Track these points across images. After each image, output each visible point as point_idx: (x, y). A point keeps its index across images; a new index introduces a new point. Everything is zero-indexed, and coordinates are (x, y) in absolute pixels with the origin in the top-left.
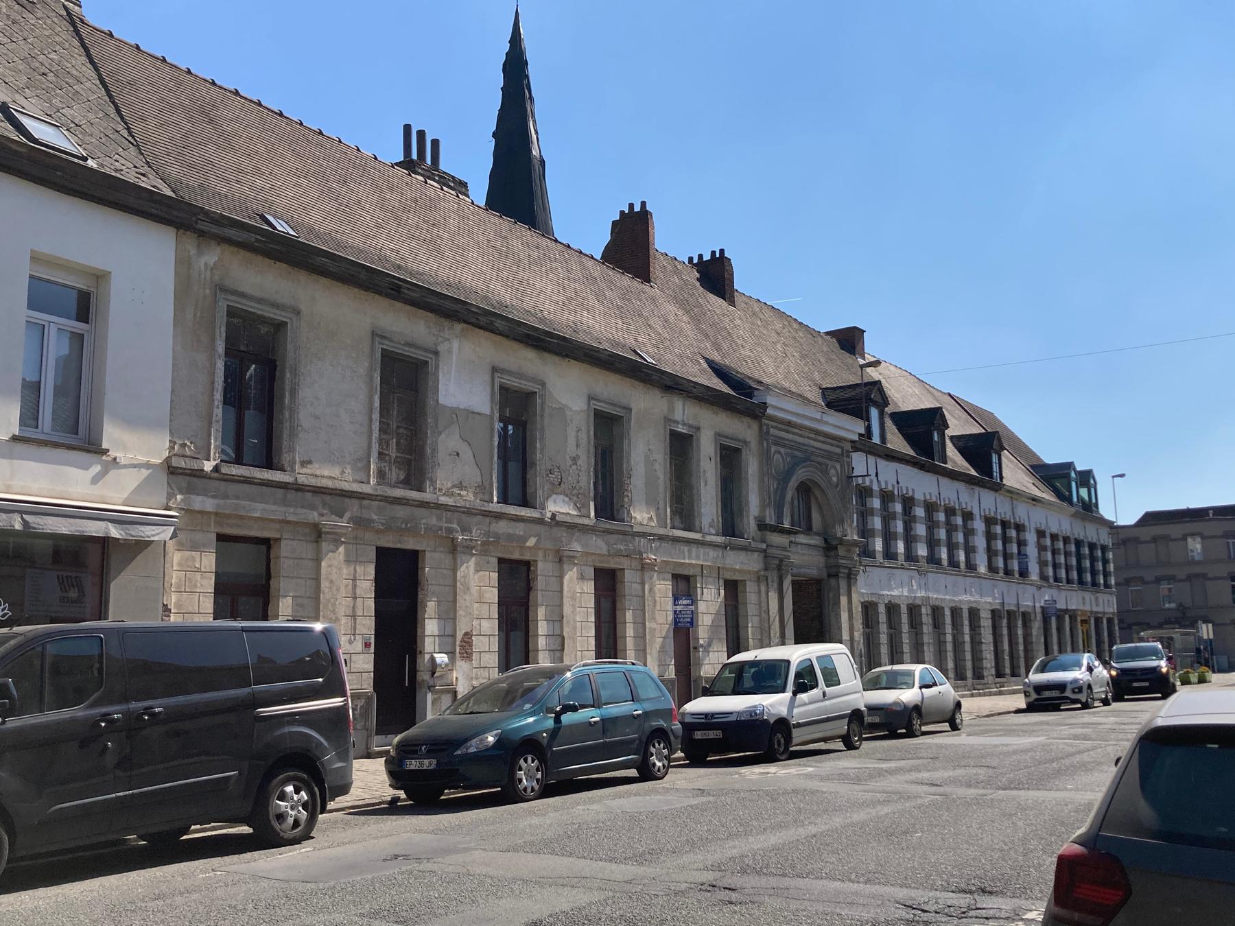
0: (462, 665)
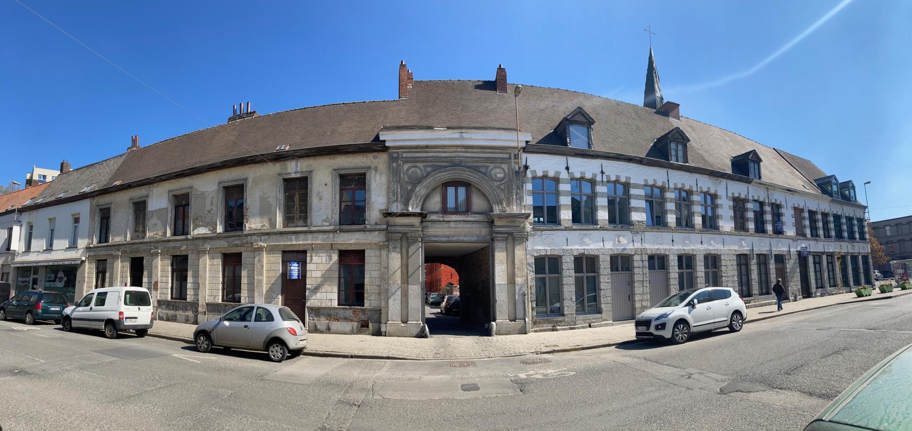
0: (154, 292)
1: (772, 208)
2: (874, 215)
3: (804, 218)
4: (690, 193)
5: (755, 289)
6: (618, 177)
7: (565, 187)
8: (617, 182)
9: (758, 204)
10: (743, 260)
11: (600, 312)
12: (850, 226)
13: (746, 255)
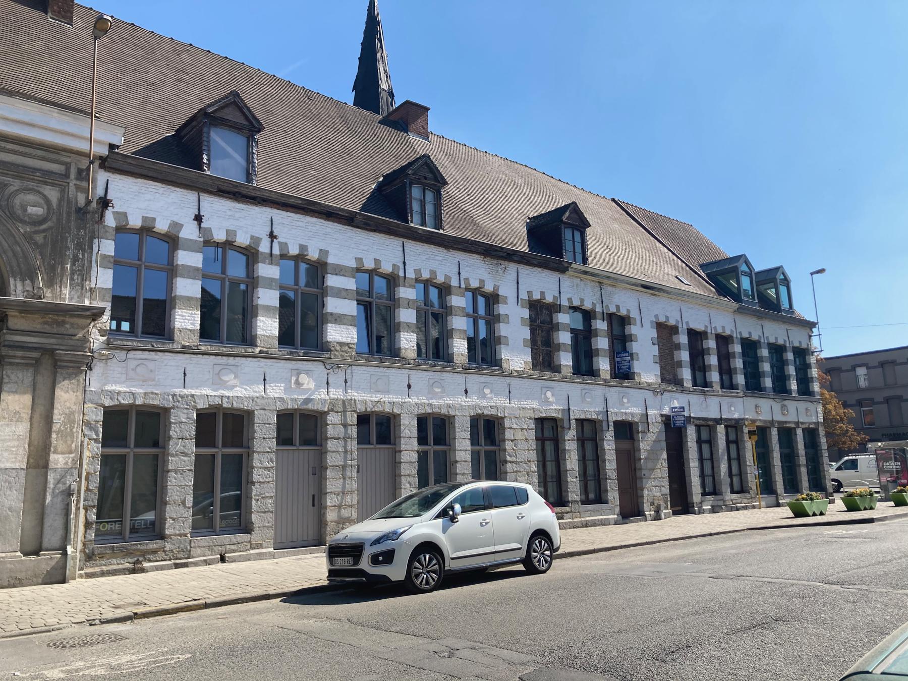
1: (610, 325)
2: (829, 344)
3: (678, 347)
4: (444, 290)
5: (574, 491)
6: (303, 248)
7: (187, 258)
8: (300, 258)
9: (579, 316)
10: (548, 430)
11: (247, 529)
12: (780, 367)
13: (554, 420)
